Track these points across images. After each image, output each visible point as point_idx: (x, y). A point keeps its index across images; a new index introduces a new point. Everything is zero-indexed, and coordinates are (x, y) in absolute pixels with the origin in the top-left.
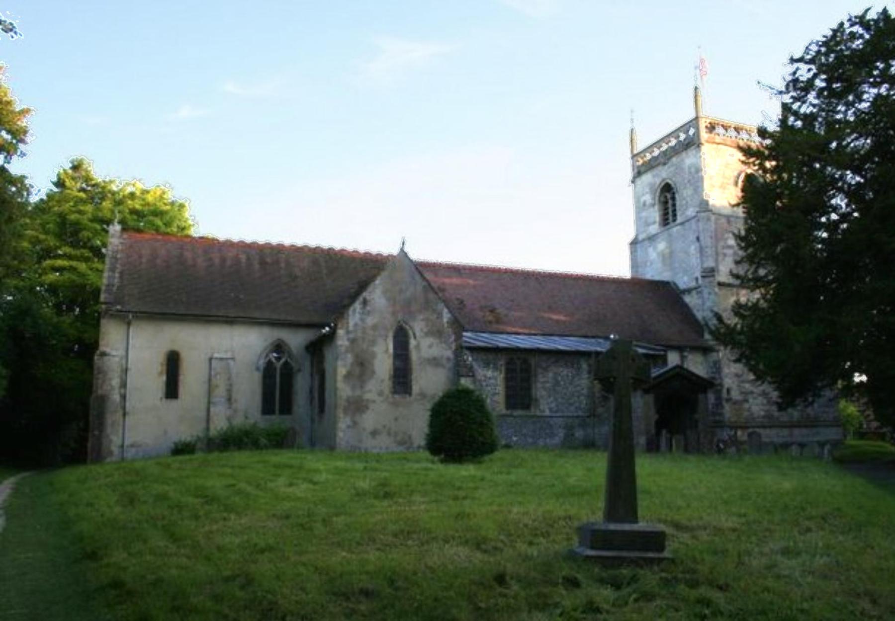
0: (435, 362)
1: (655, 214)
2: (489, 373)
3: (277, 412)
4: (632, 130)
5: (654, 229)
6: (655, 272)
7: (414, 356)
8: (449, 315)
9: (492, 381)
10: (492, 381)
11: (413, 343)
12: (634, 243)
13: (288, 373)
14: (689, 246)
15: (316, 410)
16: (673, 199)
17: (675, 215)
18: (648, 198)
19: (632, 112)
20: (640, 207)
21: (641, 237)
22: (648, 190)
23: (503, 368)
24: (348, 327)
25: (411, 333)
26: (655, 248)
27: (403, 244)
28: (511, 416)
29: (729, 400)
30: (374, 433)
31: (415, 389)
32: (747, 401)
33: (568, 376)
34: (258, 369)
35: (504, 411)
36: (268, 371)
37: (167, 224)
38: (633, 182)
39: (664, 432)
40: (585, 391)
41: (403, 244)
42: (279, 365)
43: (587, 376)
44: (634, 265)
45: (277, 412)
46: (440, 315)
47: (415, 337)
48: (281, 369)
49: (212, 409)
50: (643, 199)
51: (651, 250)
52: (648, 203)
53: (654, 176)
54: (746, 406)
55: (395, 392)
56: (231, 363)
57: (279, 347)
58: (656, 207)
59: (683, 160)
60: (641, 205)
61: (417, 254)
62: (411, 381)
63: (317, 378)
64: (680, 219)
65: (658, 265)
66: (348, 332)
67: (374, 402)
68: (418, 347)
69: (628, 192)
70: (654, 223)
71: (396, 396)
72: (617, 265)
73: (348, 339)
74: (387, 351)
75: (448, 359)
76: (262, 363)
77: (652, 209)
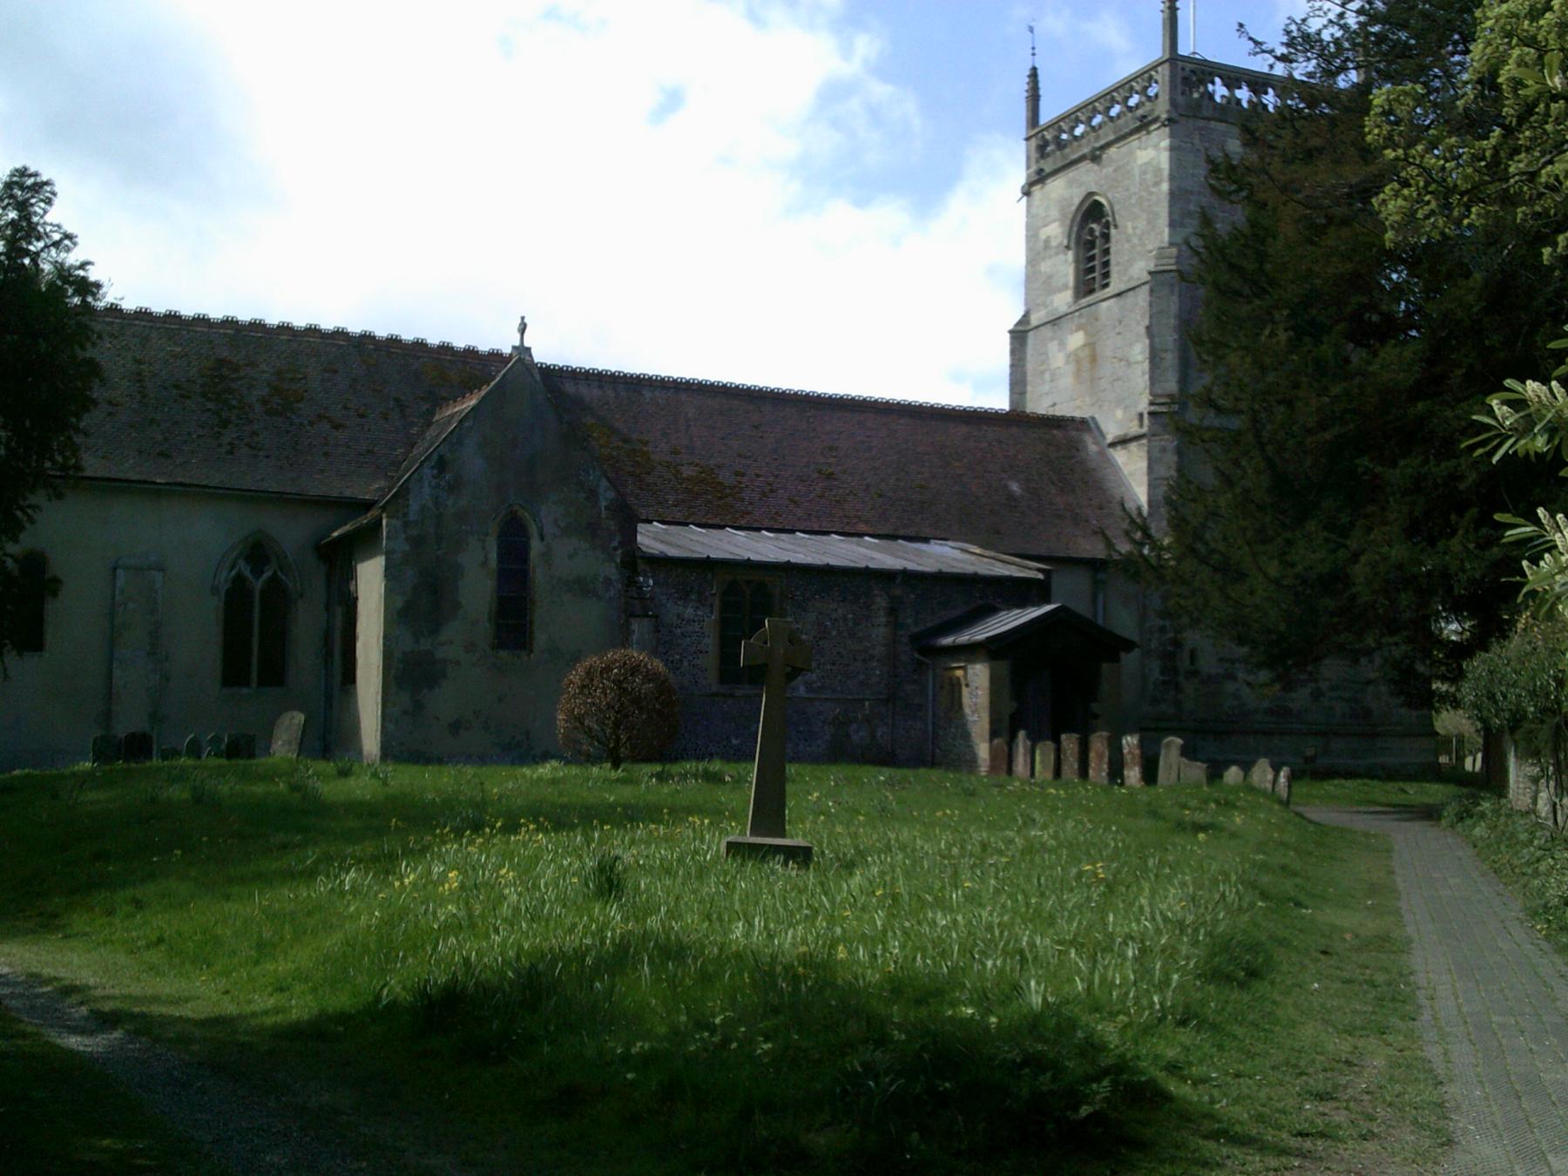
0: (582, 587)
1: (1065, 268)
2: (689, 612)
3: (254, 685)
4: (1034, 74)
5: (1063, 300)
6: (1055, 396)
7: (539, 576)
8: (611, 494)
9: (697, 627)
10: (697, 627)
11: (536, 546)
12: (1019, 336)
13: (278, 600)
14: (1131, 345)
15: (338, 679)
16: (1106, 237)
17: (1106, 275)
18: (1055, 231)
19: (1031, 30)
20: (1036, 252)
21: (1035, 319)
22: (1055, 213)
23: (717, 603)
24: (405, 515)
25: (533, 529)
26: (1062, 345)
27: (523, 328)
28: (732, 696)
29: (1193, 673)
30: (456, 727)
31: (541, 639)
32: (1232, 677)
33: (845, 618)
34: (214, 590)
35: (715, 688)
36: (236, 599)
37: (882, 1041)
38: (1027, 192)
39: (1022, 734)
40: (879, 651)
41: (523, 328)
42: (258, 585)
43: (884, 620)
44: (1018, 382)
45: (254, 685)
46: (593, 494)
47: (542, 539)
48: (263, 592)
49: (117, 673)
50: (1044, 233)
51: (1053, 347)
52: (1054, 243)
53: (1070, 183)
54: (1230, 687)
55: (500, 643)
56: (158, 576)
57: (258, 552)
58: (1070, 255)
59: (1132, 153)
60: (1041, 244)
61: (546, 352)
62: (531, 622)
63: (339, 611)
64: (1116, 285)
65: (1067, 381)
66: (406, 525)
67: (458, 663)
68: (547, 556)
69: (1017, 211)
70: (1065, 287)
71: (503, 653)
72: (973, 379)
73: (407, 539)
74: (485, 563)
75: (608, 582)
76: (225, 577)
77: (1062, 257)
